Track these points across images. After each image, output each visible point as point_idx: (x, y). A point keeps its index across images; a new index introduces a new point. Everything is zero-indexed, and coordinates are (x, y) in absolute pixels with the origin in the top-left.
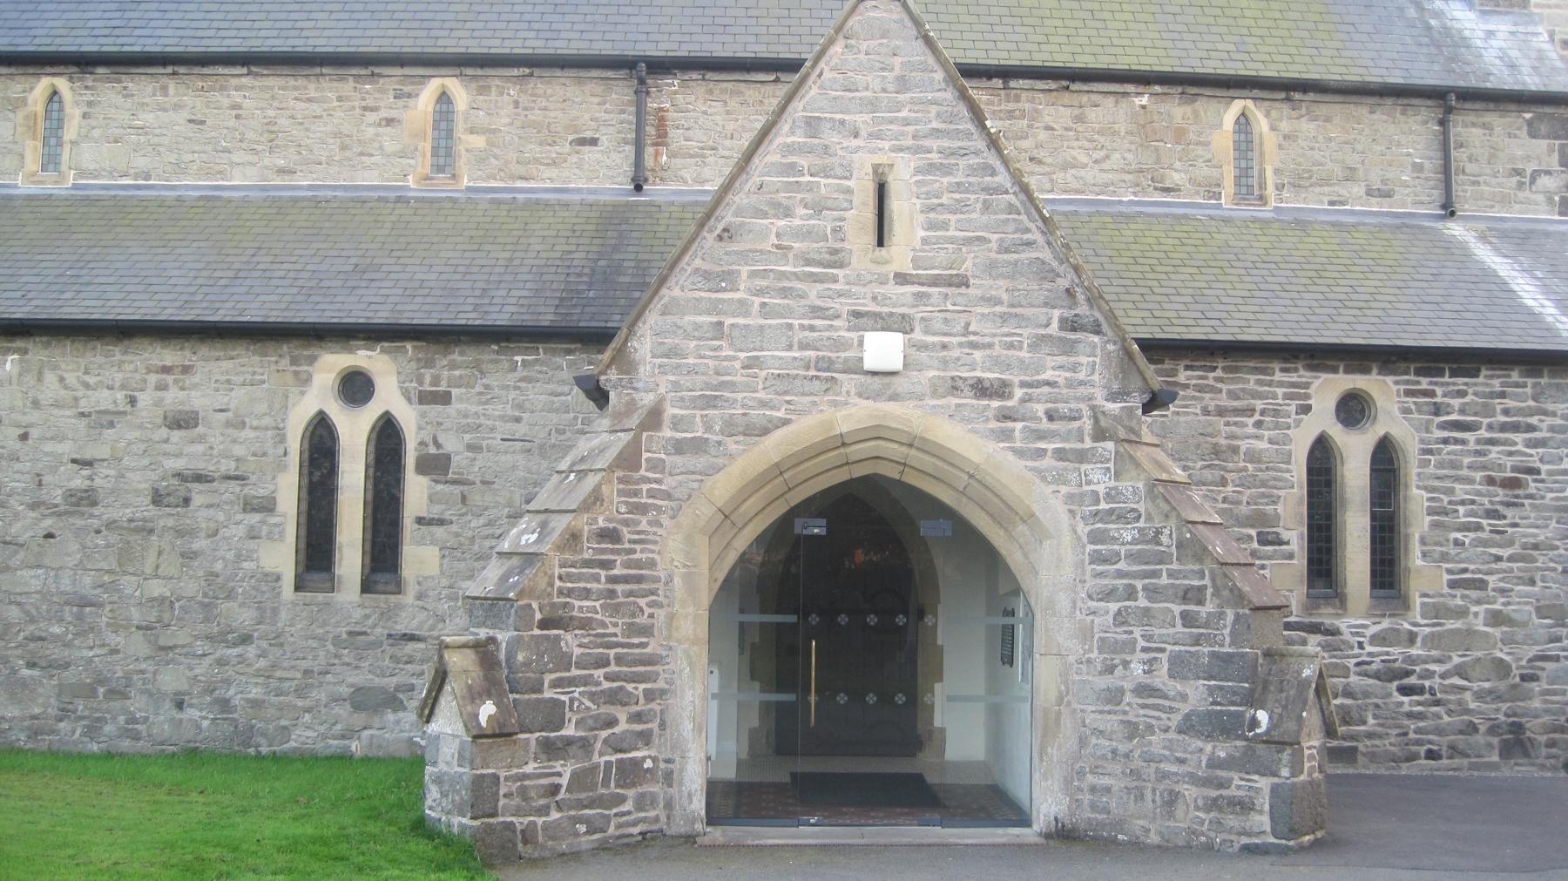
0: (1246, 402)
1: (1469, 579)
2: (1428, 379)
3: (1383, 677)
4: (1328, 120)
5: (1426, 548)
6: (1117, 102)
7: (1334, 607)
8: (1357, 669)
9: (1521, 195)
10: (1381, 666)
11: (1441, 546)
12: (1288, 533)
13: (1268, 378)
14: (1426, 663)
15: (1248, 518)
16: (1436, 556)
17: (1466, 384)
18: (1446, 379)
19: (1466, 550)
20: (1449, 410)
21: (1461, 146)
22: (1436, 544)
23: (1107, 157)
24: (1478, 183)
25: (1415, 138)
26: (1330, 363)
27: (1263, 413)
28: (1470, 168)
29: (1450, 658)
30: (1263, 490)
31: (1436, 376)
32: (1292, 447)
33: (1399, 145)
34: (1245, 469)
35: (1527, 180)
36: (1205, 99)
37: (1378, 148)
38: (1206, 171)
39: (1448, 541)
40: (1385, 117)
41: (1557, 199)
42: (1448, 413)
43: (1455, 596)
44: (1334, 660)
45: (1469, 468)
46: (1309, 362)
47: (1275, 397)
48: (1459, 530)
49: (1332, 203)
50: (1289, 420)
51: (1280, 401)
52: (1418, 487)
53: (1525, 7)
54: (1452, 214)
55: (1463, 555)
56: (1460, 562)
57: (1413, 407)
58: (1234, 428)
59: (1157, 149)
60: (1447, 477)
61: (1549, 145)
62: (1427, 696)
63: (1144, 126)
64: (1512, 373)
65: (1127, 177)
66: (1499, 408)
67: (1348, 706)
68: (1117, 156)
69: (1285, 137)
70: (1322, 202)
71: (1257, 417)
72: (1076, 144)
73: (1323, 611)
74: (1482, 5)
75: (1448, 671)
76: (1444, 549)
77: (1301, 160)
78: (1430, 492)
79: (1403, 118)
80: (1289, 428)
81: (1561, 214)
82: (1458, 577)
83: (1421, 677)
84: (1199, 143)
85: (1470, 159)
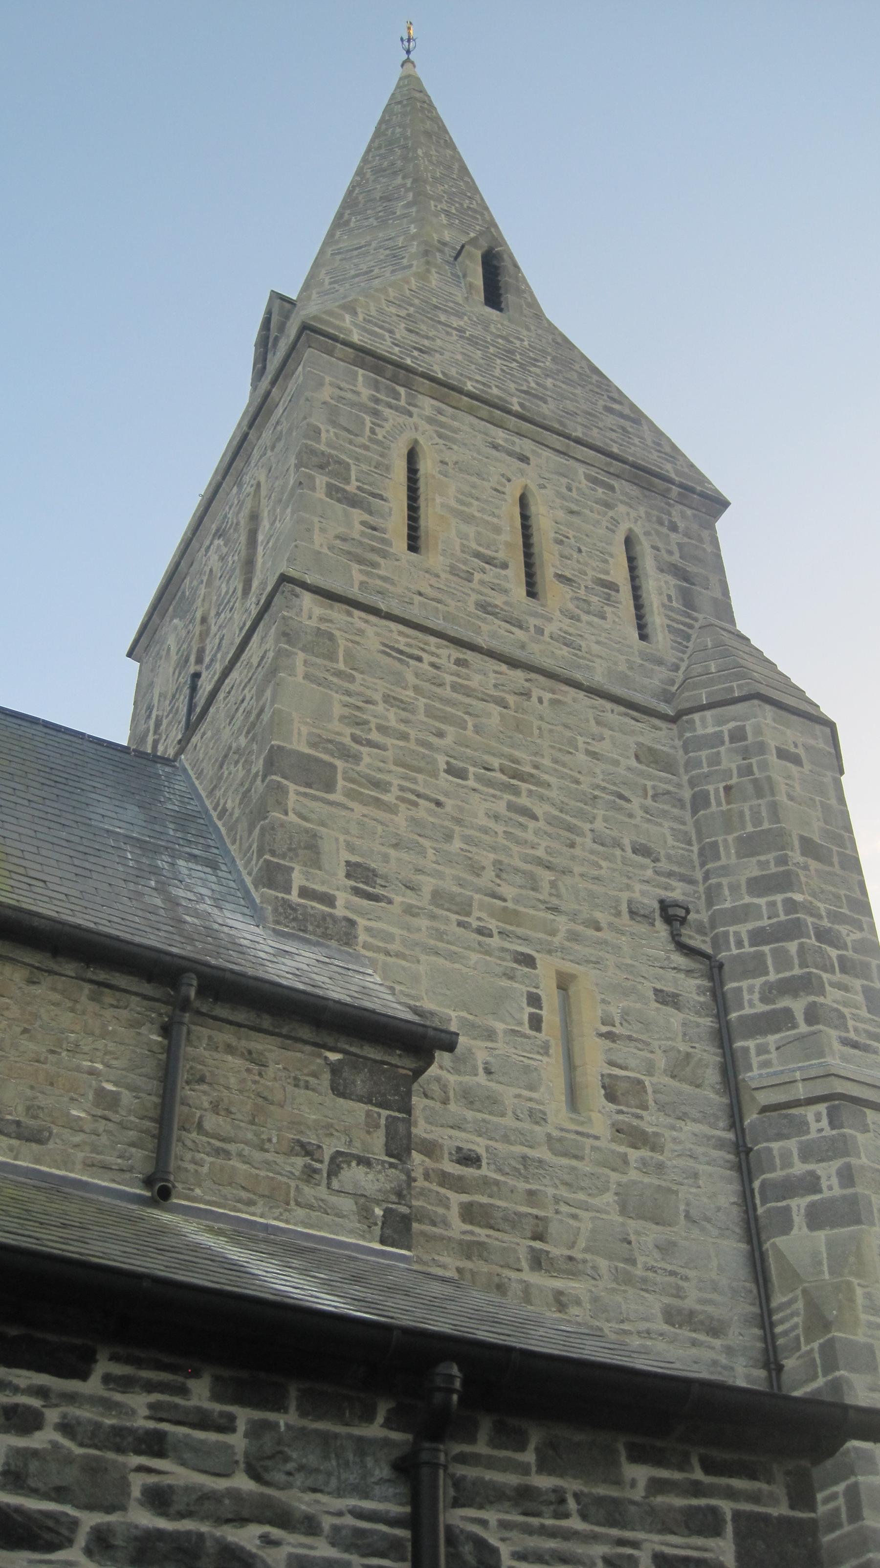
9: (308, 1191)
17: (42, 1392)
21: (202, 1080)
24: (227, 1154)
25: (111, 1046)
28: (211, 1122)
33: (75, 1049)
35: (324, 1167)
37: (32, 1046)
40: (56, 997)
41: (378, 1212)
53: (347, 944)
54: (165, 1194)
61: (368, 1114)
64: (193, 1384)
66: (137, 1483)
74: (277, 922)
79: (92, 1007)
81: (382, 1242)
85: (216, 1107)
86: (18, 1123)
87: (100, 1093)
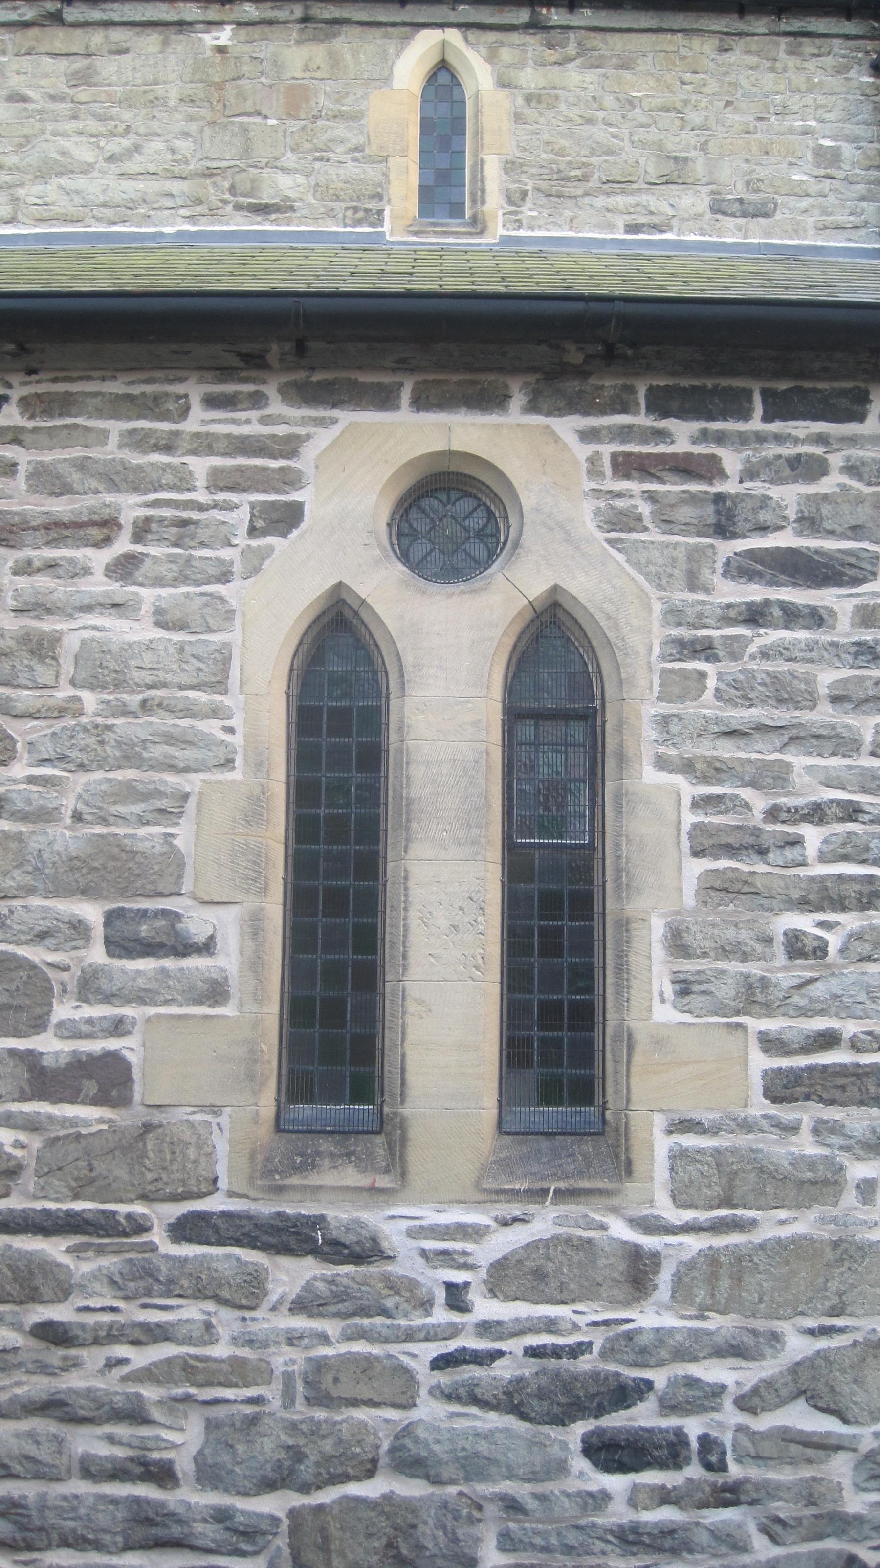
0: (90, 501)
1: (841, 1071)
2: (696, 426)
3: (537, 1406)
4: (625, 65)
5: (690, 966)
6: (165, 43)
7: (365, 1164)
8: (444, 1378)
10: (529, 1368)
11: (745, 957)
12: (211, 914)
13: (165, 426)
14: (683, 1354)
15: (74, 863)
16: (726, 991)
17: (821, 439)
18: (756, 424)
19: (831, 971)
20: (765, 517)
22: (725, 952)
23: (137, 148)
25: (821, 99)
26: (367, 378)
27: (141, 532)
29: (775, 1338)
30: (130, 774)
31: (724, 416)
32: (233, 636)
33: (783, 112)
34: (72, 708)
36: (358, 30)
38: (352, 169)
39: (768, 941)
40: (753, 60)
42: (763, 529)
43: (793, 1129)
44: (360, 1347)
45: (836, 700)
46: (300, 375)
47: (184, 482)
48: (804, 904)
49: (633, 228)
50: (226, 554)
51: (201, 496)
52: (662, 763)
55: (819, 990)
56: (805, 1012)
57: (645, 509)
58: (43, 581)
59: (245, 129)
60: (762, 728)
62: (694, 1471)
63: (220, 87)
65: (175, 186)
67: (410, 1506)
68: (158, 145)
69: (528, 99)
70: (611, 227)
71: (123, 545)
72: (71, 126)
73: (327, 1178)
75: (769, 1383)
76: (754, 969)
77: (564, 142)
78: (704, 779)
79: (792, 62)
80: (225, 578)
82: (802, 1061)
83: (669, 1407)
84: (338, 116)
86: (741, 201)
87: (819, 152)
